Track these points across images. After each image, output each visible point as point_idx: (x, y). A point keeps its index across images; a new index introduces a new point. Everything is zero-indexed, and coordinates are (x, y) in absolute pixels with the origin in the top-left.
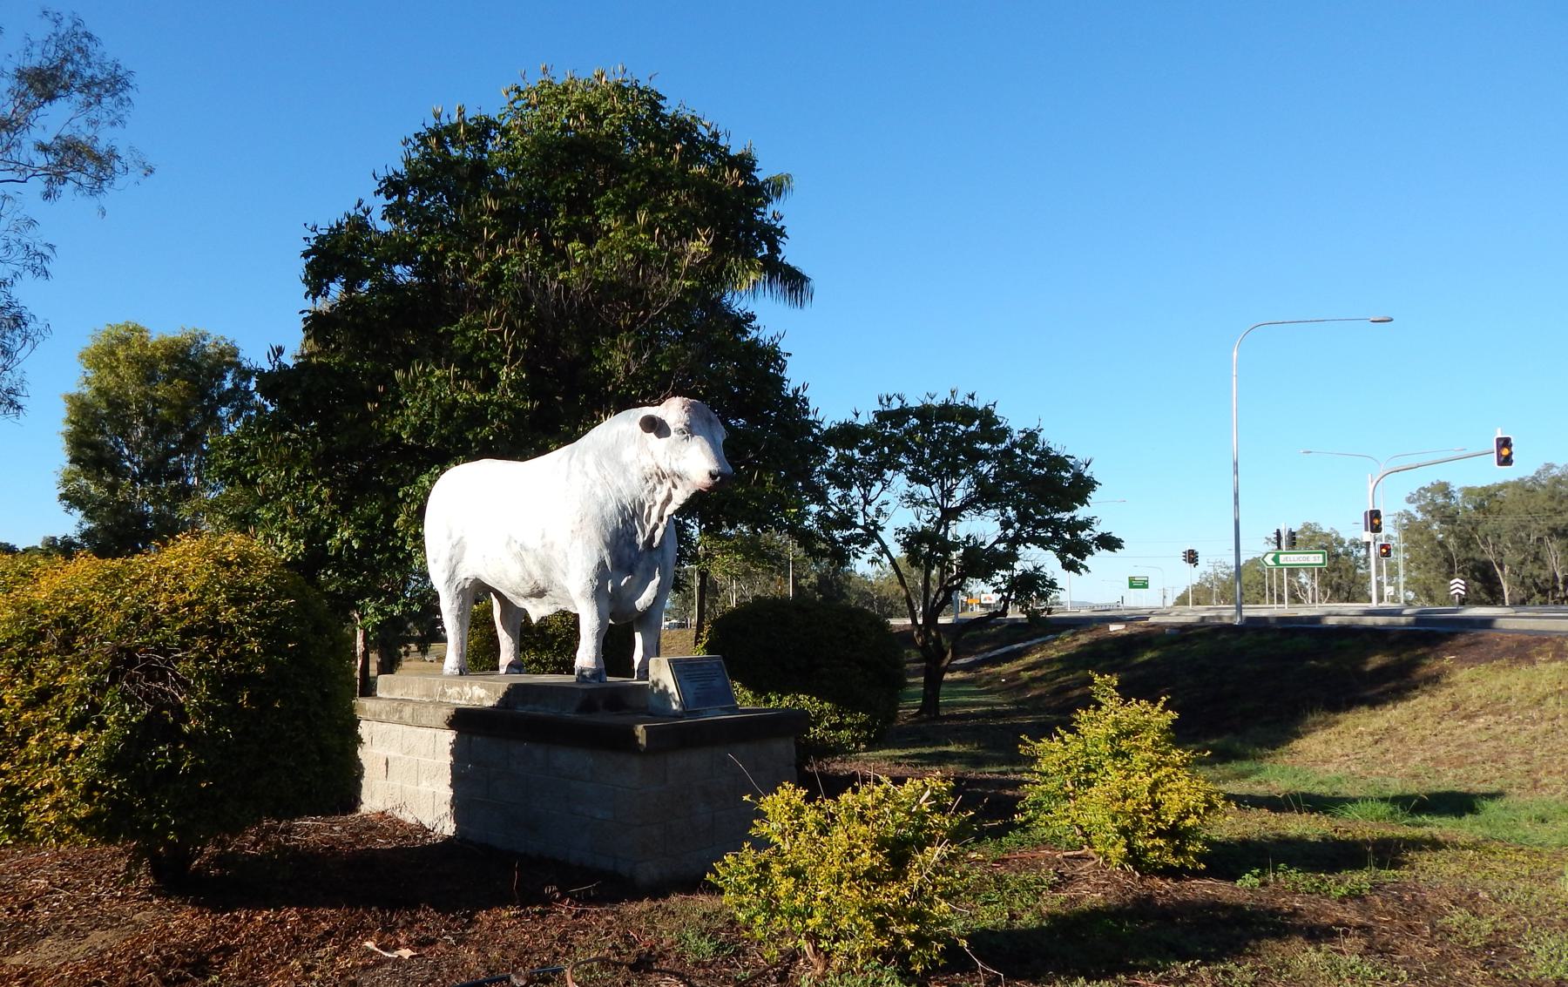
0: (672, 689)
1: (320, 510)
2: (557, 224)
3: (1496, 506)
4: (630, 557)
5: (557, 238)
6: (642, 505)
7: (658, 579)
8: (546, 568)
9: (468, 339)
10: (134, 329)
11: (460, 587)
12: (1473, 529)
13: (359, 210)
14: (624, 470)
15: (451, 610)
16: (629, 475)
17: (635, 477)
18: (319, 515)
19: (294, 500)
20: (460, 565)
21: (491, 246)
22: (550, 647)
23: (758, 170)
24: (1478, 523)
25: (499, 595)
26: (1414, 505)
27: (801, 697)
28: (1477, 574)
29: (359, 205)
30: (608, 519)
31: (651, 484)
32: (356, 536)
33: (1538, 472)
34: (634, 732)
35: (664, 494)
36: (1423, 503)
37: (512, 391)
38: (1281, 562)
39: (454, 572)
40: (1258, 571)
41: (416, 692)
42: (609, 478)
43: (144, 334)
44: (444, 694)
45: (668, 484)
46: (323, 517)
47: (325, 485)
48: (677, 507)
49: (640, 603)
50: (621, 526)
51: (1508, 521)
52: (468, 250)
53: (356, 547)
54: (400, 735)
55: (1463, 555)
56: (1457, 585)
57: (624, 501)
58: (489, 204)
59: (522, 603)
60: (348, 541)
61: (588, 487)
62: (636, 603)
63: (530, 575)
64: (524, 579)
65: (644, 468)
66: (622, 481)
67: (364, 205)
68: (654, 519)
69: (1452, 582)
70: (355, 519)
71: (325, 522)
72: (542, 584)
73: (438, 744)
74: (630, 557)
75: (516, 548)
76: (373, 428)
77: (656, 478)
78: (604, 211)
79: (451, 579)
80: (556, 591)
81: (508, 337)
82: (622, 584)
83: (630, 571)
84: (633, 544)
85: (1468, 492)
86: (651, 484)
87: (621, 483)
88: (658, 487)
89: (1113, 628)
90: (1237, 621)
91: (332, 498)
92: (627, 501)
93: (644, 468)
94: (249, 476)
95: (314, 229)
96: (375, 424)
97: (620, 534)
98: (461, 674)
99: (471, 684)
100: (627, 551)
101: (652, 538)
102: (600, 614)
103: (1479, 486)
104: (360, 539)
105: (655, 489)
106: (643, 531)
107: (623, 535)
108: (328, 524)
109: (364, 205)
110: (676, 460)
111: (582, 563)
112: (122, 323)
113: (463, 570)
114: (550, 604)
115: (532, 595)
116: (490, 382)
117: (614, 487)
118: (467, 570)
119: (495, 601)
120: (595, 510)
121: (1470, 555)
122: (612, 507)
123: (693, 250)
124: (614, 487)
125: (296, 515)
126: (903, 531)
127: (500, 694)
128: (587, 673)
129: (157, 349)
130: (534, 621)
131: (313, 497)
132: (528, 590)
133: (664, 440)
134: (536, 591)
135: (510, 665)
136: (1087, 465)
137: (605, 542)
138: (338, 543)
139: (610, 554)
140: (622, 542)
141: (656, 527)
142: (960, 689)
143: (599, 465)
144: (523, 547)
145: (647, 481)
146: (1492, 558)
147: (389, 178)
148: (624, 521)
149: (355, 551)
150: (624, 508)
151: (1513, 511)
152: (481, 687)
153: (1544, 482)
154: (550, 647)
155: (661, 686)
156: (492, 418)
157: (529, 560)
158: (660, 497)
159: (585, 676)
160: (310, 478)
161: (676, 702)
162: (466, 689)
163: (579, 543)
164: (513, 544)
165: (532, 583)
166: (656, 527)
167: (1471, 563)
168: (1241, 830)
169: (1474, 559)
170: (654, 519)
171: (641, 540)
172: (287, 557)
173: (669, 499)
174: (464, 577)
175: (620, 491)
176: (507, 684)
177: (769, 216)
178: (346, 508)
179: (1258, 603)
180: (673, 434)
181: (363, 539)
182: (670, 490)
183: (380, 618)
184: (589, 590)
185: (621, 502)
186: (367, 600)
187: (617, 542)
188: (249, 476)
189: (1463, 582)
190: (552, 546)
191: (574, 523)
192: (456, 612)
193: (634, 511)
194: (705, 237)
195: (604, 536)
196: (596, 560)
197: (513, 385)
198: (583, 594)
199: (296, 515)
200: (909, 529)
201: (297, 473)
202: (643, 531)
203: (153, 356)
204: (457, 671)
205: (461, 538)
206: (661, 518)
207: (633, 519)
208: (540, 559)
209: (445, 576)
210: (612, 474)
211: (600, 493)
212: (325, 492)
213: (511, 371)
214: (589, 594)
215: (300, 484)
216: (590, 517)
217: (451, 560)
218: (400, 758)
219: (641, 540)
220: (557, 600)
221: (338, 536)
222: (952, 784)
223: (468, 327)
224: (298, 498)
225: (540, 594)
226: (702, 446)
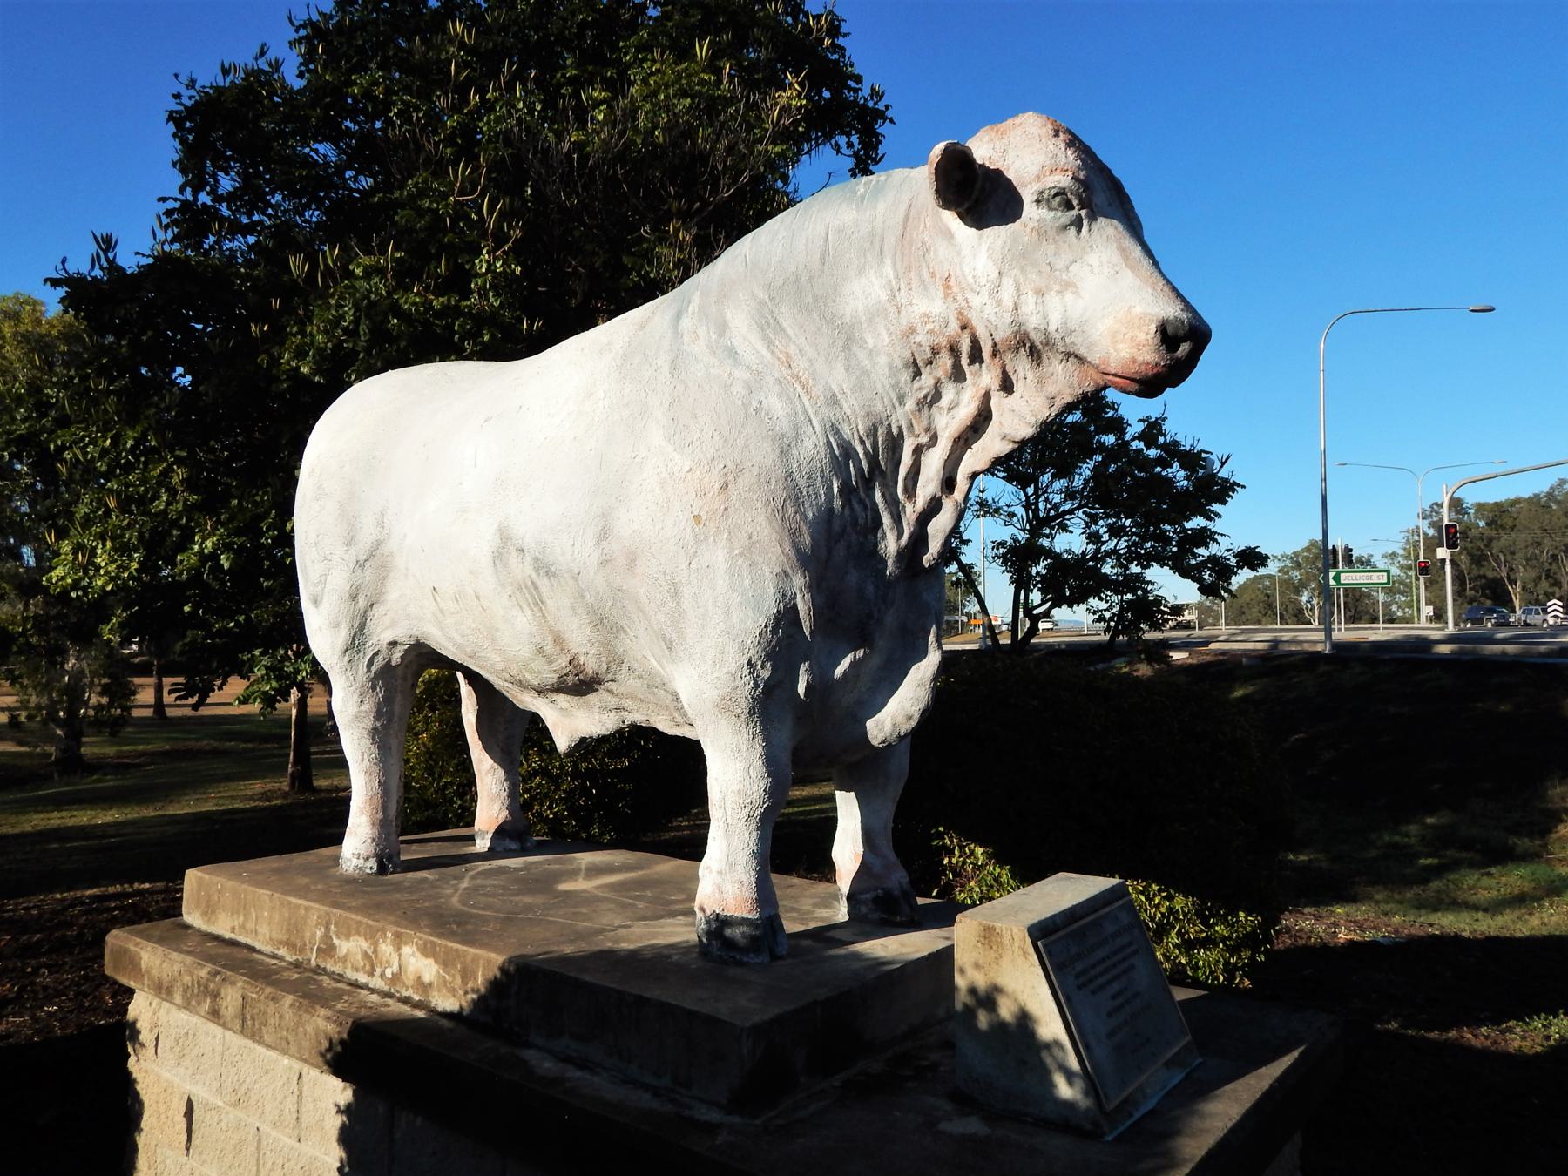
0: (1051, 1027)
1: (168, 503)
2: (563, 76)
3: (1509, 522)
5: (563, 96)
6: (895, 444)
8: (605, 624)
9: (421, 213)
10: (26, 302)
11: (379, 663)
12: (1486, 546)
13: (261, 61)
14: (848, 338)
15: (357, 718)
16: (862, 356)
17: (883, 360)
18: (165, 512)
19: (127, 486)
20: (377, 611)
21: (462, 90)
23: (845, 35)
24: (1490, 540)
25: (474, 678)
26: (1426, 522)
28: (1487, 592)
29: (262, 53)
30: (802, 483)
31: (927, 380)
32: (227, 547)
33: (1551, 488)
35: (966, 410)
36: (1435, 519)
37: (497, 295)
38: (1342, 582)
39: (362, 627)
40: (1259, 589)
41: (264, 930)
42: (801, 365)
43: (38, 308)
44: (328, 950)
45: (986, 377)
46: (172, 515)
47: (180, 462)
48: (1004, 448)
49: (880, 725)
50: (837, 503)
51: (1522, 538)
52: (425, 95)
53: (226, 566)
54: (219, 1049)
55: (1475, 572)
56: (1555, 613)
57: (846, 431)
58: (459, 30)
59: (529, 702)
60: (214, 557)
61: (738, 389)
62: (870, 724)
63: (558, 641)
64: (541, 651)
65: (912, 330)
66: (840, 371)
67: (271, 56)
68: (928, 486)
69: (1549, 604)
70: (231, 520)
71: (174, 523)
72: (591, 665)
73: (308, 1106)
75: (522, 569)
76: (260, 366)
77: (945, 361)
78: (635, 57)
79: (356, 642)
80: (627, 683)
81: (490, 213)
82: (839, 672)
83: (861, 637)
84: (872, 555)
85: (1480, 507)
86: (927, 380)
87: (837, 378)
88: (948, 394)
89: (1176, 656)
90: (1326, 649)
91: (189, 484)
92: (854, 431)
93: (912, 330)
94: (52, 447)
95: (192, 84)
96: (263, 359)
97: (837, 526)
98: (382, 870)
99: (397, 936)
100: (853, 577)
102: (771, 761)
103: (1492, 502)
104: (235, 552)
105: (937, 396)
106: (897, 521)
108: (180, 528)
109: (271, 56)
110: (1040, 293)
111: (728, 612)
112: (10, 294)
113: (387, 621)
114: (606, 710)
115: (561, 688)
116: (459, 281)
117: (817, 391)
118: (393, 624)
119: (466, 691)
120: (764, 455)
121: (1481, 573)
122: (812, 448)
123: (783, 101)
124: (817, 391)
125: (123, 511)
126: (1002, 544)
127: (480, 981)
128: (735, 933)
129: (54, 326)
130: (562, 744)
131: (160, 484)
132: (551, 678)
133: (997, 235)
134: (571, 680)
135: (501, 832)
136: (1223, 464)
137: (798, 551)
138: (194, 560)
140: (840, 551)
141: (934, 507)
143: (768, 326)
144: (544, 567)
145: (917, 373)
146: (1504, 575)
147: (310, 23)
148: (846, 490)
149: (226, 573)
150: (848, 451)
151: (1529, 528)
152: (427, 951)
153: (1559, 498)
155: (1006, 1011)
156: (462, 339)
157: (559, 604)
158: (951, 419)
159: (729, 944)
160: (153, 450)
161: (1069, 1076)
162: (386, 948)
163: (718, 555)
164: (513, 559)
165: (563, 662)
166: (934, 507)
167: (1483, 581)
169: (1484, 576)
170: (928, 486)
171: (890, 544)
172: (106, 584)
173: (982, 420)
174: (388, 636)
175: (833, 400)
176: (498, 959)
177: (866, 92)
178: (211, 504)
179: (1259, 623)
180: (1030, 210)
181: (239, 553)
182: (987, 397)
183: (274, 684)
184: (744, 690)
185: (838, 432)
186: (257, 653)
187: (830, 551)
188: (52, 447)
189: (1561, 604)
190: (632, 560)
191: (702, 494)
192: (369, 722)
193: (873, 458)
194: (799, 84)
195: (794, 535)
196: (770, 607)
197: (503, 283)
198: (725, 705)
199: (123, 511)
200: (1010, 542)
201: (130, 443)
202: (897, 521)
203: (49, 334)
204: (372, 864)
205: (378, 544)
206: (949, 484)
207: (868, 483)
208: (590, 599)
209: (343, 635)
210: (810, 352)
211: (776, 406)
212: (181, 473)
213: (496, 259)
214: (743, 705)
215: (137, 460)
216: (747, 478)
217: (354, 597)
218: (217, 1108)
219: (890, 544)
220: (627, 703)
221: (196, 547)
223: (422, 193)
224: (133, 485)
225: (580, 685)
226: (1122, 250)
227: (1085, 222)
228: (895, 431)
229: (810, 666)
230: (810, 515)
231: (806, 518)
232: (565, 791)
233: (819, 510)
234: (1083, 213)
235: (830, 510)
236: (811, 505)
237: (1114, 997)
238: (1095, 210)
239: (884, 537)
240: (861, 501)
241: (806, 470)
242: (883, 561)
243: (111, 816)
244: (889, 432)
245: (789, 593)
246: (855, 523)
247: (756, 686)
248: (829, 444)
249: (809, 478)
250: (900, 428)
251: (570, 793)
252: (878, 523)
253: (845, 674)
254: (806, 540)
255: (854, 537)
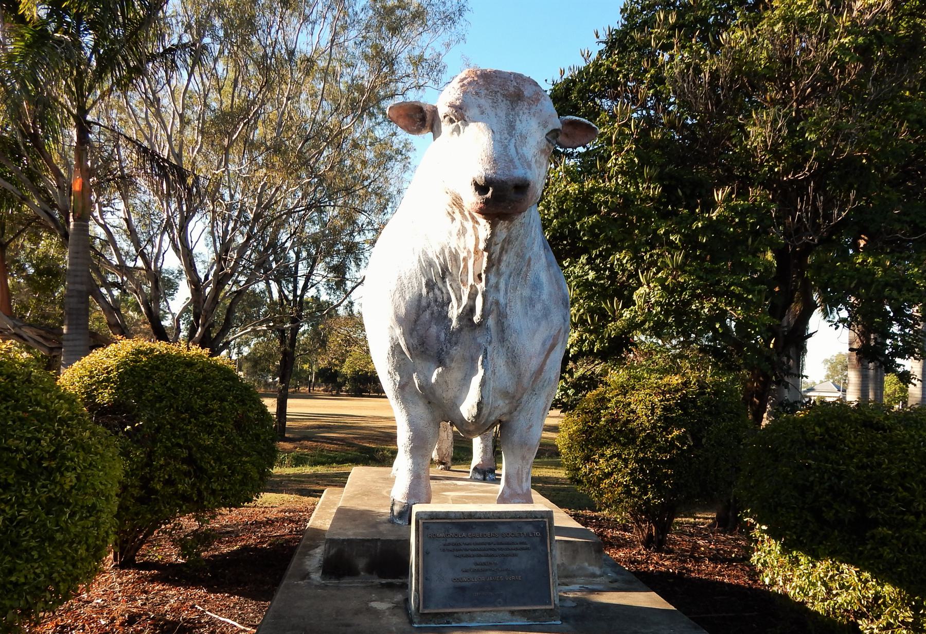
4: (438, 337)
7: (481, 372)
22: (632, 441)
27: (844, 566)
30: (406, 282)
34: (458, 408)
50: (424, 291)
74: (438, 337)
84: (444, 318)
97: (424, 303)
100: (434, 329)
101: (471, 310)
106: (459, 299)
107: (429, 305)
139: (404, 334)
140: (427, 315)
142: (368, 432)
150: (430, 264)
154: (632, 441)
168: (100, 352)
171: (454, 312)
187: (418, 316)
195: (397, 308)
202: (459, 299)
219: (454, 312)
222: (165, 352)
227: (461, 127)
228: (454, 251)
229: (417, 375)
230: (407, 298)
231: (405, 299)
232: (630, 469)
233: (413, 295)
234: (459, 123)
235: (421, 295)
236: (409, 293)
237: (477, 564)
238: (467, 119)
239: (452, 307)
240: (439, 289)
241: (408, 274)
242: (451, 320)
243: (343, 435)
244: (451, 252)
245: (394, 337)
246: (436, 301)
247: (395, 384)
248: (420, 261)
249: (410, 279)
250: (456, 250)
251: (633, 471)
252: (450, 300)
253: (436, 380)
254: (403, 311)
255: (436, 308)
